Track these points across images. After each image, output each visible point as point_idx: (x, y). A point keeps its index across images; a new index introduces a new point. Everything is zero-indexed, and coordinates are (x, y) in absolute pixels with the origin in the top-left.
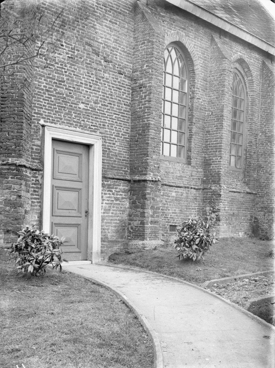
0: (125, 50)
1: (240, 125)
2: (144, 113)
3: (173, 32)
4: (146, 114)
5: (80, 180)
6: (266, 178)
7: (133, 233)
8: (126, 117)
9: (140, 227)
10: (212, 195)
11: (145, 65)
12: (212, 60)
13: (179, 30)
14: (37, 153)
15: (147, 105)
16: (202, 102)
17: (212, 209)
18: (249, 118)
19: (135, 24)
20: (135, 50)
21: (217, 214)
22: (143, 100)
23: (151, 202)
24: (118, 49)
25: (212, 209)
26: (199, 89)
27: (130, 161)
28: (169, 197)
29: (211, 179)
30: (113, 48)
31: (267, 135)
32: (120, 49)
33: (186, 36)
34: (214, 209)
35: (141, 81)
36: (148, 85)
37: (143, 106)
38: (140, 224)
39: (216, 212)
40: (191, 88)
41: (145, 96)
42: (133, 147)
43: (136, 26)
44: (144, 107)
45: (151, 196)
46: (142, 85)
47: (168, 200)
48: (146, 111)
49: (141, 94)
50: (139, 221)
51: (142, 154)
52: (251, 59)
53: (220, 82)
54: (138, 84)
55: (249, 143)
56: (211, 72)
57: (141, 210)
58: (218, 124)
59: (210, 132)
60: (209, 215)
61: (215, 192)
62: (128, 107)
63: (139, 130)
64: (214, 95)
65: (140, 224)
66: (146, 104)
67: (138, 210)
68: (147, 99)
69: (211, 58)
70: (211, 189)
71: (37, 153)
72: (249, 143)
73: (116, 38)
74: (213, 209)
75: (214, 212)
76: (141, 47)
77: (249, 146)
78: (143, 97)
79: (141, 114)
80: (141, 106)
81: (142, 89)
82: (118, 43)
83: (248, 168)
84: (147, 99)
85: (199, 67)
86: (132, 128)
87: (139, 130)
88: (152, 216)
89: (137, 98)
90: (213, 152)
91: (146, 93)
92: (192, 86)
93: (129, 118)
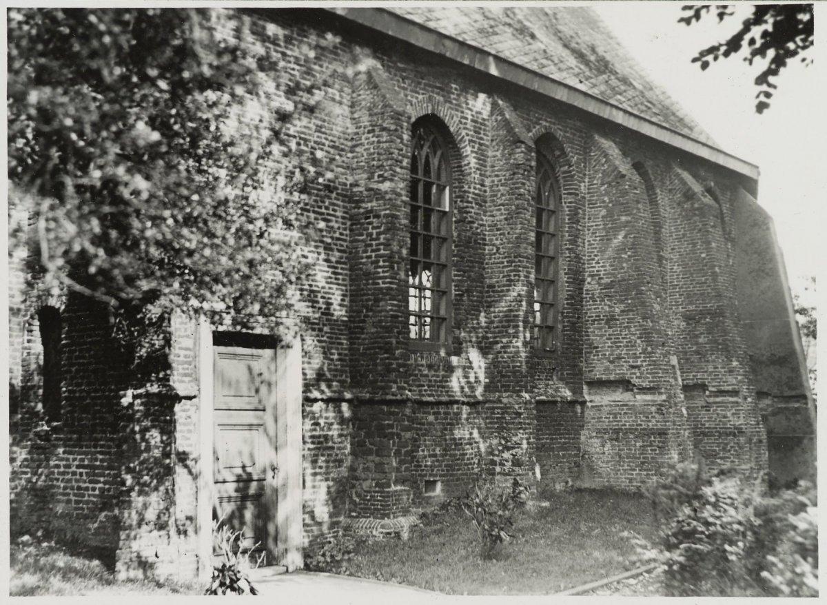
0: (337, 144)
1: (549, 242)
2: (375, 268)
3: (420, 97)
4: (380, 270)
5: (261, 407)
6: (604, 370)
7: (360, 504)
8: (341, 274)
9: (375, 492)
10: (503, 413)
11: (376, 174)
12: (494, 143)
13: (433, 92)
14: (186, 363)
15: (382, 252)
16: (477, 228)
17: (503, 442)
18: (568, 249)
19: (353, 92)
20: (354, 143)
21: (514, 452)
22: (374, 243)
23: (394, 442)
24: (324, 145)
25: (503, 442)
26: (471, 203)
27: (351, 360)
28: (423, 424)
29: (499, 381)
30: (315, 142)
31: (603, 281)
32: (327, 143)
33: (446, 101)
34: (507, 441)
35: (369, 205)
36: (383, 213)
37: (373, 254)
38: (376, 487)
39: (514, 448)
40: (456, 202)
41: (379, 234)
42: (356, 333)
43: (354, 95)
44: (376, 256)
45: (395, 430)
46: (371, 211)
47: (420, 433)
48: (381, 263)
49: (370, 230)
50: (373, 480)
51: (375, 348)
52: (566, 132)
53: (511, 189)
54: (362, 210)
55: (567, 299)
56: (493, 166)
57: (377, 459)
58: (511, 271)
59: (494, 287)
60: (498, 456)
61: (509, 408)
62: (345, 255)
63: (368, 300)
64: (501, 214)
65: (376, 487)
66: (379, 250)
67: (371, 458)
68: (382, 240)
69: (492, 140)
70: (500, 402)
71: (186, 363)
72: (567, 299)
73: (320, 123)
74: (507, 441)
75: (508, 449)
76: (367, 139)
77: (568, 304)
78: (374, 236)
79: (371, 268)
80: (369, 254)
81: (371, 220)
82: (324, 133)
83: (567, 349)
84: (382, 240)
85: (497, 258)
86: (351, 295)
87: (368, 300)
88: (398, 470)
89: (361, 238)
90: (503, 327)
91: (379, 227)
92: (457, 197)
93: (346, 275)
